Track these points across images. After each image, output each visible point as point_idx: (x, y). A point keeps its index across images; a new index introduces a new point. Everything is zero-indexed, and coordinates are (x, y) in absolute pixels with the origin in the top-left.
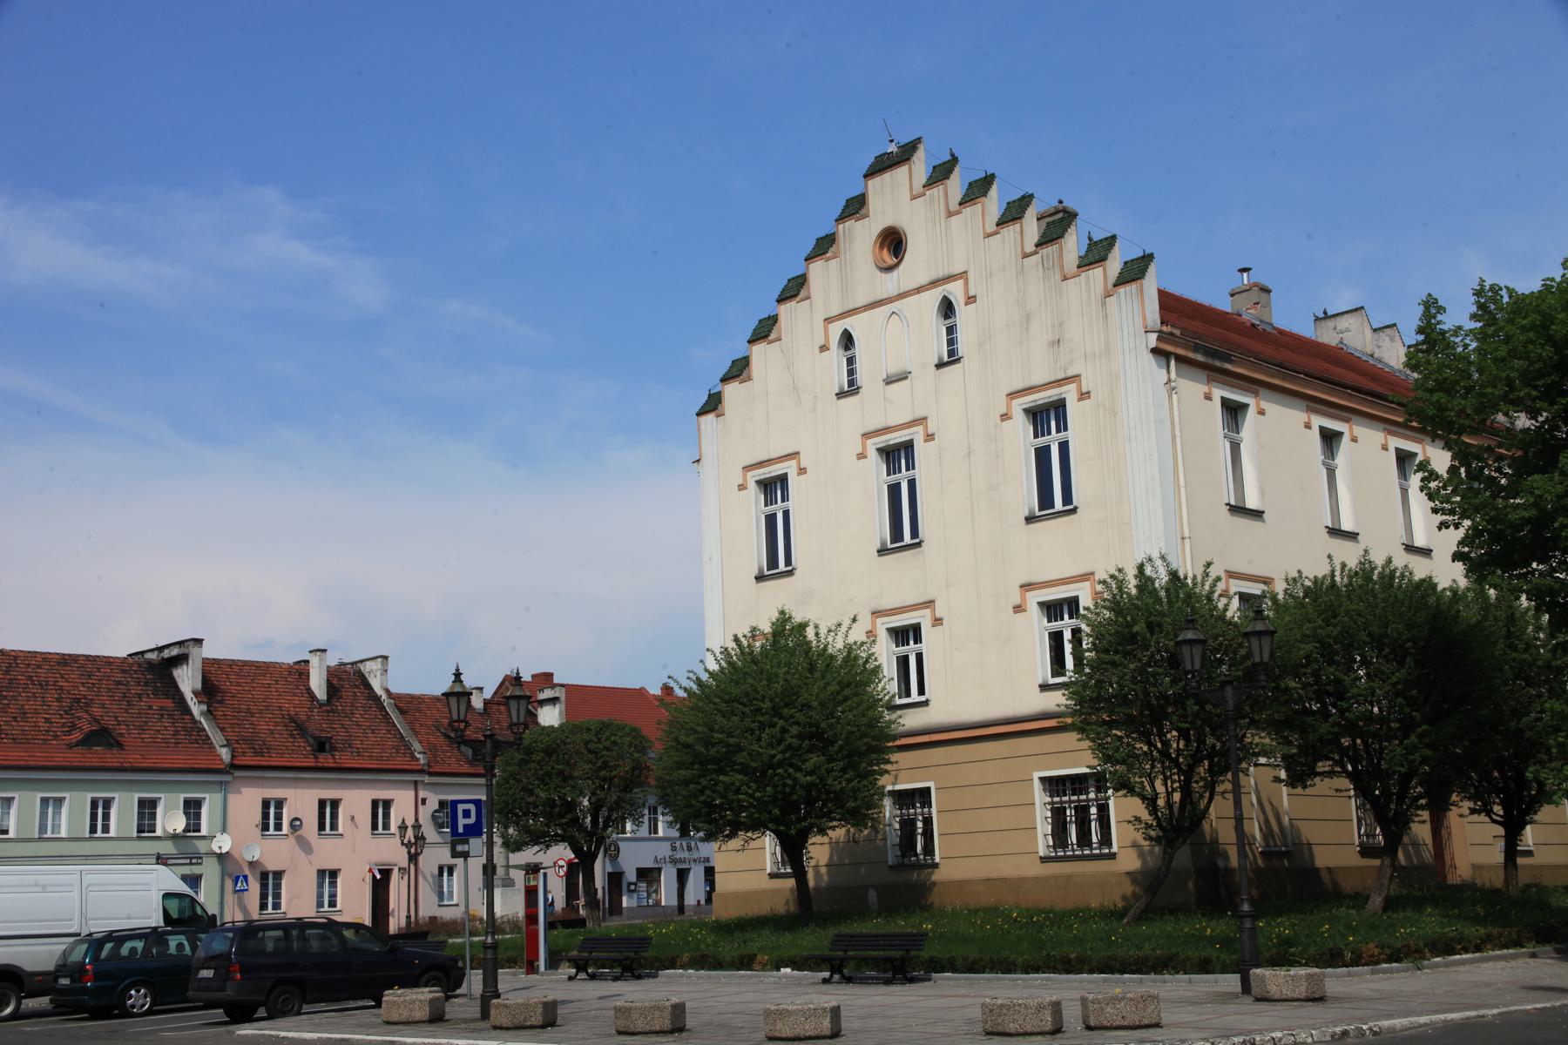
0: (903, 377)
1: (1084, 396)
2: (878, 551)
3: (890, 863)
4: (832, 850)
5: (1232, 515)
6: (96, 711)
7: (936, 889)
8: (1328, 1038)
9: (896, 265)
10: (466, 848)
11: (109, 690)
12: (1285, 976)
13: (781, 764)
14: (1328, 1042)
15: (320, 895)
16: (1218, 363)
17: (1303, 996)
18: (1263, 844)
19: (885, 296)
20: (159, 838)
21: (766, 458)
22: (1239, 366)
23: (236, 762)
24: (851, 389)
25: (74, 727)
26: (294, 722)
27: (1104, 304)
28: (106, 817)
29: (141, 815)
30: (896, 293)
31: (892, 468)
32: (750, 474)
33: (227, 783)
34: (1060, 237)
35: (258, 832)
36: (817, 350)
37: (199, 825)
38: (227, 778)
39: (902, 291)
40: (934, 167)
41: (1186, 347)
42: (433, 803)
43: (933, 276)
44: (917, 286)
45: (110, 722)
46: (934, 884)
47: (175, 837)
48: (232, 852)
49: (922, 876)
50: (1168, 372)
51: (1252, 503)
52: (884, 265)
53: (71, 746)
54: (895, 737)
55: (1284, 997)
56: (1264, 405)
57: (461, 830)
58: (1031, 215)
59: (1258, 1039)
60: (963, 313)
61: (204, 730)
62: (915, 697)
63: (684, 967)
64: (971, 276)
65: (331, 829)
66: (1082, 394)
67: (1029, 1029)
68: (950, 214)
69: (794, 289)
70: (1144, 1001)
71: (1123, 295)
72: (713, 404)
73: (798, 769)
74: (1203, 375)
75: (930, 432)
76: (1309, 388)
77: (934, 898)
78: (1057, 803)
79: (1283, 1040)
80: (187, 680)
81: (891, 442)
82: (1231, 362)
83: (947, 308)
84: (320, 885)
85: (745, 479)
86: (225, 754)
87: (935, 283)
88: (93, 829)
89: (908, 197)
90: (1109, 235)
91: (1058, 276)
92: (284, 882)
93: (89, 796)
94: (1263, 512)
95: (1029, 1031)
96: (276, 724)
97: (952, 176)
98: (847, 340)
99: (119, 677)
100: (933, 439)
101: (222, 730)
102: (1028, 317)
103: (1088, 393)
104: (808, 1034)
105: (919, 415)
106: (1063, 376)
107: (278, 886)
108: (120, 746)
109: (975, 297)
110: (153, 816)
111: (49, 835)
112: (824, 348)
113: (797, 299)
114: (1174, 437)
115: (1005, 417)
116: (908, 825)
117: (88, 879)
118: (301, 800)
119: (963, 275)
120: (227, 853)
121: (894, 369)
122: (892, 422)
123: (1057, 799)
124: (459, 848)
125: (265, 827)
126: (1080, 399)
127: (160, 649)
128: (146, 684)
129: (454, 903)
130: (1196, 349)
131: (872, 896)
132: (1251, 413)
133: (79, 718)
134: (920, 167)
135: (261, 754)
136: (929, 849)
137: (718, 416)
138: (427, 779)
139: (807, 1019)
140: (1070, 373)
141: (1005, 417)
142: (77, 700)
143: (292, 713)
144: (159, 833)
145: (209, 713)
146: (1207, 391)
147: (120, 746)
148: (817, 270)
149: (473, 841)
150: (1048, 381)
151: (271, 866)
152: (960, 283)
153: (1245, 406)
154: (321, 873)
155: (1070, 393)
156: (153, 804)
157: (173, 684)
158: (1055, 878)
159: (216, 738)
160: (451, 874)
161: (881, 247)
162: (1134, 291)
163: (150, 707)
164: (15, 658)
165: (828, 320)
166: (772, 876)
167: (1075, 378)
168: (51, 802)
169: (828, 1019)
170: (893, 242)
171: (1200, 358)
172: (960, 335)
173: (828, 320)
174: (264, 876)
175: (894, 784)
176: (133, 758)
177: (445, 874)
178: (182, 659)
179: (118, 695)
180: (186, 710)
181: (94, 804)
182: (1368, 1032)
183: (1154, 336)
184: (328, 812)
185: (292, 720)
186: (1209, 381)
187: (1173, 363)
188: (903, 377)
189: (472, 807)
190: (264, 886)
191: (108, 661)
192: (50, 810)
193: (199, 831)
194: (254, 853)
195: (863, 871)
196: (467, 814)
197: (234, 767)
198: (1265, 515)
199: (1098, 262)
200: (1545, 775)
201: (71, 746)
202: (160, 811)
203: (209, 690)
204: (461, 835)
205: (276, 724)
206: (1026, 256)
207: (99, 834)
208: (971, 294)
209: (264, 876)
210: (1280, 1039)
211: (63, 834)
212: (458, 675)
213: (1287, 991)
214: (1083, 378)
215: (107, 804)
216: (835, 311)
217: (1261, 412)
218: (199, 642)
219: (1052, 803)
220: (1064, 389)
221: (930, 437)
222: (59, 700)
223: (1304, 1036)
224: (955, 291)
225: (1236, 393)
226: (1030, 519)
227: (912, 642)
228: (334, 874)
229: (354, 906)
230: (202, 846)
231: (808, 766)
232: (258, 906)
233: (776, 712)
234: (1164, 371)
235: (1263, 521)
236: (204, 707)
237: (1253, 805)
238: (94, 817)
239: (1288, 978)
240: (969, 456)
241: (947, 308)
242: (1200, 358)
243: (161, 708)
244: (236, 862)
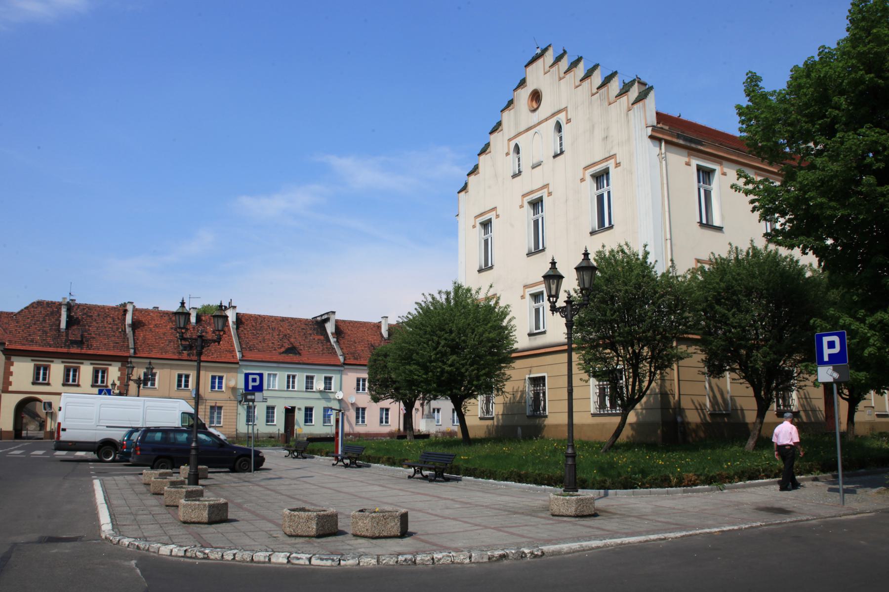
0: (539, 164)
2: (527, 255)
3: (527, 414)
4: (504, 407)
5: (702, 228)
6: (292, 340)
7: (546, 428)
8: (485, 560)
9: (537, 108)
10: (253, 397)
11: (299, 332)
12: (563, 499)
13: (436, 360)
14: (485, 562)
15: (381, 419)
16: (693, 145)
17: (573, 513)
18: (711, 409)
19: (533, 124)
20: (314, 392)
21: (484, 211)
22: (707, 148)
23: (346, 362)
25: (282, 346)
27: (627, 115)
28: (293, 382)
29: (307, 382)
30: (537, 122)
31: (536, 212)
32: (477, 220)
33: (342, 371)
34: (607, 83)
35: (355, 391)
36: (505, 155)
37: (313, 386)
38: (342, 369)
41: (672, 136)
43: (553, 111)
44: (546, 117)
45: (297, 344)
46: (545, 426)
47: (320, 392)
48: (344, 399)
49: (541, 421)
50: (661, 149)
51: (717, 222)
52: (533, 109)
53: (280, 353)
54: (515, 351)
55: (561, 514)
56: (726, 170)
57: (250, 388)
58: (581, 65)
61: (335, 349)
62: (542, 330)
63: (383, 463)
64: (569, 109)
65: (363, 390)
66: (617, 164)
67: (299, 532)
68: (560, 79)
70: (385, 519)
72: (464, 188)
73: (444, 363)
74: (685, 152)
75: (550, 191)
76: (755, 162)
77: (545, 433)
78: (601, 385)
79: (442, 561)
80: (330, 328)
81: (534, 198)
82: (702, 145)
83: (559, 127)
85: (475, 223)
86: (341, 359)
87: (553, 115)
88: (288, 387)
89: (543, 73)
90: (632, 79)
91: (607, 103)
92: (366, 412)
93: (287, 373)
94: (722, 228)
95: (299, 534)
96: (365, 347)
97: (562, 60)
98: (517, 149)
99: (303, 326)
101: (342, 349)
102: (593, 126)
103: (620, 163)
104: (193, 520)
105: (545, 184)
106: (608, 156)
107: (363, 413)
108: (300, 354)
109: (570, 119)
110: (312, 383)
111: (271, 388)
112: (507, 154)
113: (498, 131)
114: (662, 184)
115: (582, 180)
116: (537, 395)
117: (148, 404)
120: (342, 399)
121: (535, 161)
122: (535, 188)
123: (601, 383)
124: (249, 397)
125: (358, 389)
126: (616, 167)
127: (322, 316)
128: (314, 330)
129: (221, 425)
130: (678, 137)
131: (519, 430)
132: (717, 174)
133: (285, 342)
134: (549, 57)
135: (357, 359)
136: (544, 409)
137: (466, 193)
139: (192, 511)
140: (612, 154)
141: (582, 180)
142: (286, 336)
143: (373, 343)
144: (314, 390)
145: (338, 342)
146: (687, 161)
147: (300, 354)
149: (257, 394)
150: (602, 158)
151: (361, 405)
152: (564, 113)
153: (713, 171)
155: (611, 164)
156: (312, 378)
157: (325, 329)
158: (597, 425)
159: (339, 352)
160: (438, 411)
161: (532, 100)
162: (641, 106)
163: (314, 339)
164: (264, 318)
166: (481, 419)
167: (613, 156)
168: (272, 376)
169: (207, 512)
170: (536, 96)
171: (681, 142)
173: (510, 140)
174: (358, 409)
175: (529, 374)
176: (304, 359)
177: (436, 412)
178: (327, 320)
180: (329, 341)
181: (289, 377)
182: (528, 555)
183: (650, 129)
185: (372, 345)
186: (689, 155)
187: (663, 144)
188: (539, 164)
189: (258, 377)
190: (358, 413)
191: (300, 320)
192: (272, 378)
193: (331, 389)
194: (353, 400)
195: (516, 418)
196: (254, 380)
197: (345, 364)
198: (723, 229)
199: (624, 93)
200: (812, 368)
201: (280, 353)
202: (315, 381)
203: (338, 332)
204: (250, 390)
205: (365, 347)
206: (593, 95)
207: (291, 389)
208: (569, 118)
209: (358, 409)
210: (439, 560)
211: (277, 388)
212: (183, 304)
213: (563, 509)
214: (617, 156)
215: (294, 377)
217: (724, 174)
218: (334, 313)
219: (599, 385)
220: (609, 162)
222: (278, 335)
223: (462, 558)
224: (562, 117)
225: (705, 162)
226: (593, 233)
227: (541, 301)
230: (331, 396)
231: (449, 362)
232: (265, 421)
233: (433, 333)
234: (658, 149)
235: (723, 233)
236: (335, 340)
237: (706, 388)
238: (288, 382)
239: (565, 501)
240: (566, 202)
241: (559, 127)
242: (681, 142)
244: (345, 403)
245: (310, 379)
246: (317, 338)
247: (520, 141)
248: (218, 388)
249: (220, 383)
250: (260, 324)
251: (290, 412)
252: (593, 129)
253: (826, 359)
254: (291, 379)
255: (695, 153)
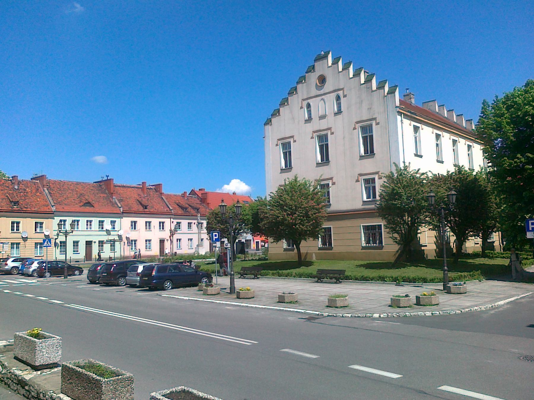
1: (377, 124)
6: (87, 197)
11: (89, 192)
15: (146, 246)
24: (310, 119)
25: (81, 201)
26: (139, 201)
30: (323, 93)
38: (121, 215)
39: (325, 92)
40: (334, 59)
42: (175, 223)
43: (334, 89)
45: (90, 200)
57: (214, 240)
59: (472, 309)
60: (343, 100)
69: (293, 91)
71: (389, 97)
82: (416, 116)
84: (146, 244)
98: (309, 106)
99: (92, 188)
100: (333, 134)
102: (362, 101)
105: (330, 127)
112: (302, 108)
118: (141, 221)
119: (342, 89)
138: (173, 216)
140: (374, 117)
141: (355, 129)
148: (299, 87)
152: (342, 91)
154: (146, 241)
156: (103, 222)
165: (304, 100)
167: (375, 119)
170: (322, 80)
172: (342, 105)
173: (304, 100)
176: (96, 209)
179: (92, 193)
184: (148, 224)
187: (402, 115)
201: (81, 206)
207: (89, 229)
216: (305, 97)
221: (332, 133)
222: (77, 194)
224: (341, 93)
228: (150, 241)
229: (155, 250)
240: (344, 138)
241: (338, 98)
243: (103, 197)
245: (101, 223)
246: (102, 195)
247: (310, 101)
248: (16, 230)
249: (18, 227)
250: (63, 187)
251: (89, 244)
252: (362, 103)
253: (530, 229)
254: (89, 223)
255: (426, 124)
